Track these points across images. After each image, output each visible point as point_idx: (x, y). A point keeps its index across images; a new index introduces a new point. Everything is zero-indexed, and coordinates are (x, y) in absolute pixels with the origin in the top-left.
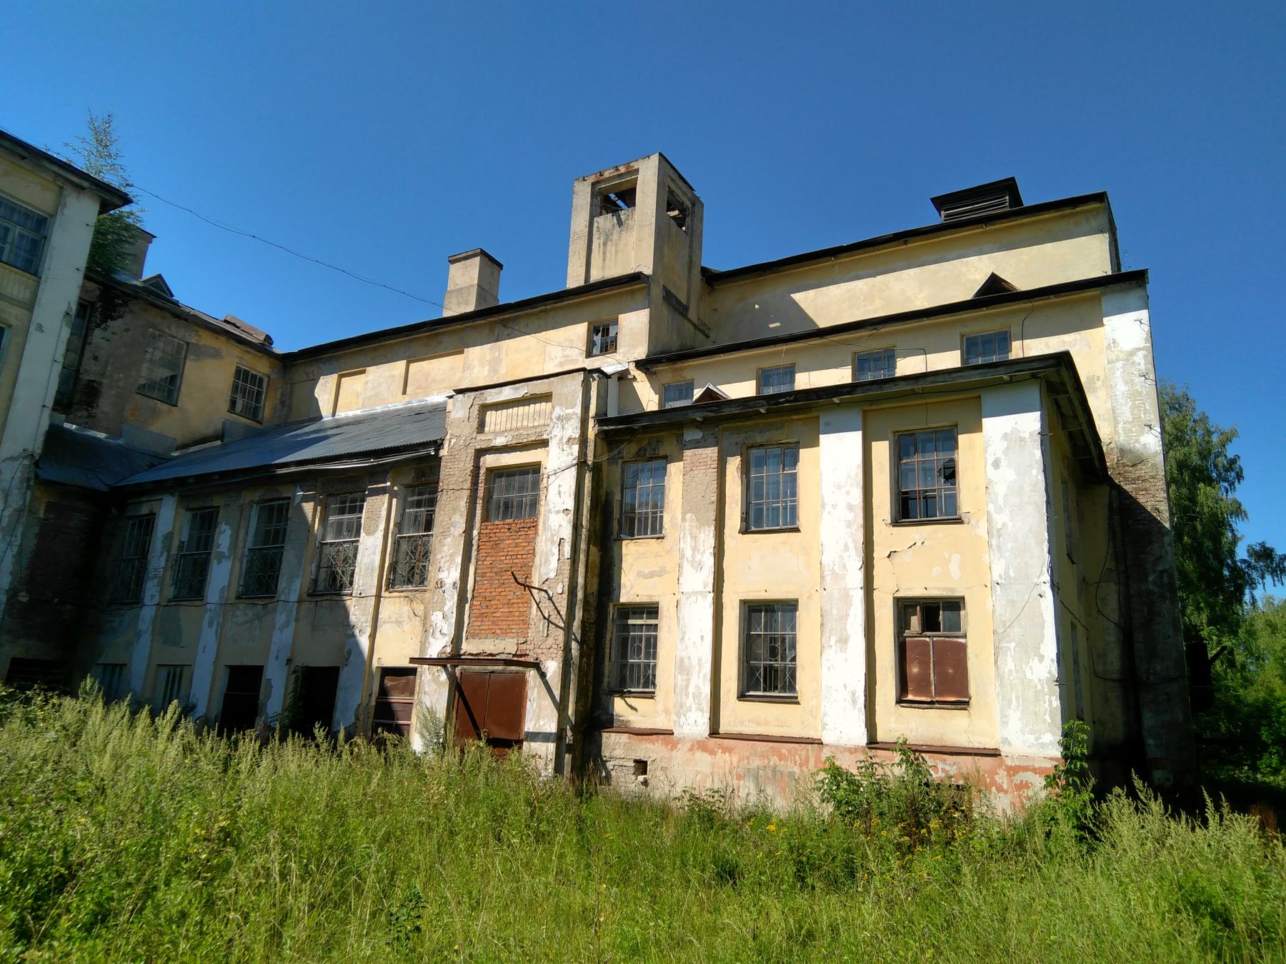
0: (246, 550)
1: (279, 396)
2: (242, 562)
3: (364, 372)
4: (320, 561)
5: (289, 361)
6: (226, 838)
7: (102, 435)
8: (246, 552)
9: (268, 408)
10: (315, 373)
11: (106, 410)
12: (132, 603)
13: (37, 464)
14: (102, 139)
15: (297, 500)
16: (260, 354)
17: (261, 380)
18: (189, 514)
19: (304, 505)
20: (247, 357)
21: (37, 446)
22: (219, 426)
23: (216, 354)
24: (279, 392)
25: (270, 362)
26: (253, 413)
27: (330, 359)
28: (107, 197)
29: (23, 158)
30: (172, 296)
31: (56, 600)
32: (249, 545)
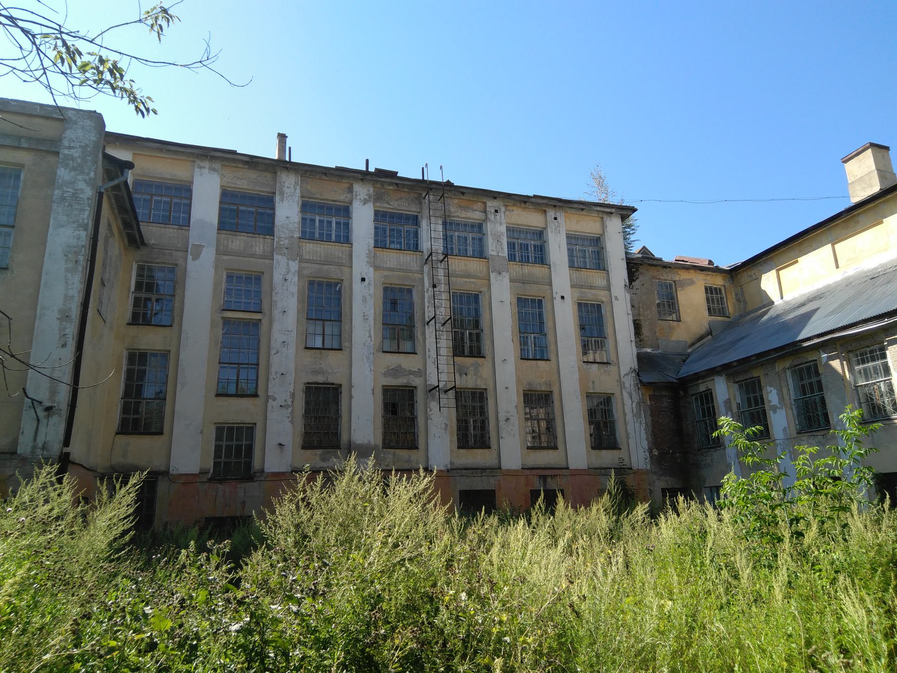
0: (792, 400)
1: (734, 296)
2: (792, 409)
3: (797, 262)
4: (859, 399)
5: (734, 272)
6: (321, 569)
7: (649, 350)
8: (793, 403)
9: (731, 306)
10: (757, 274)
11: (647, 334)
12: (716, 447)
13: (638, 375)
14: (600, 182)
15: (824, 361)
16: (715, 274)
17: (720, 289)
18: (736, 386)
19: (831, 362)
20: (709, 278)
21: (634, 364)
22: (707, 326)
23: (692, 282)
24: (733, 294)
25: (722, 276)
26: (722, 312)
27: (765, 262)
28: (624, 212)
29: (582, 210)
30: (654, 256)
31: (671, 451)
32: (793, 397)
